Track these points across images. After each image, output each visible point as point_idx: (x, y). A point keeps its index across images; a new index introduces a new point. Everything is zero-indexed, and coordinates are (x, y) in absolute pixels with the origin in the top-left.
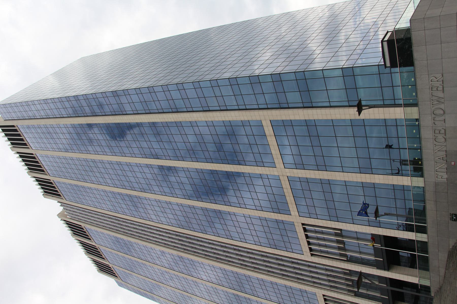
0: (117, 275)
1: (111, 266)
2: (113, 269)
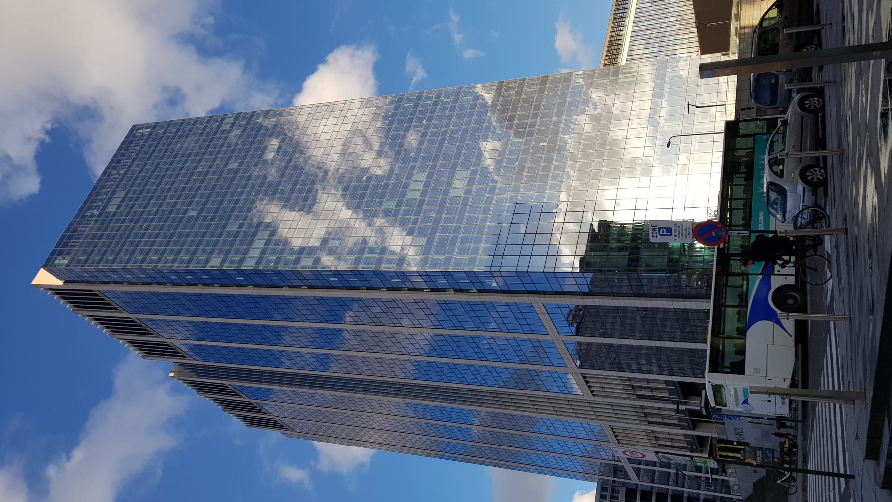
0: (286, 427)
1: (276, 418)
2: (280, 422)
